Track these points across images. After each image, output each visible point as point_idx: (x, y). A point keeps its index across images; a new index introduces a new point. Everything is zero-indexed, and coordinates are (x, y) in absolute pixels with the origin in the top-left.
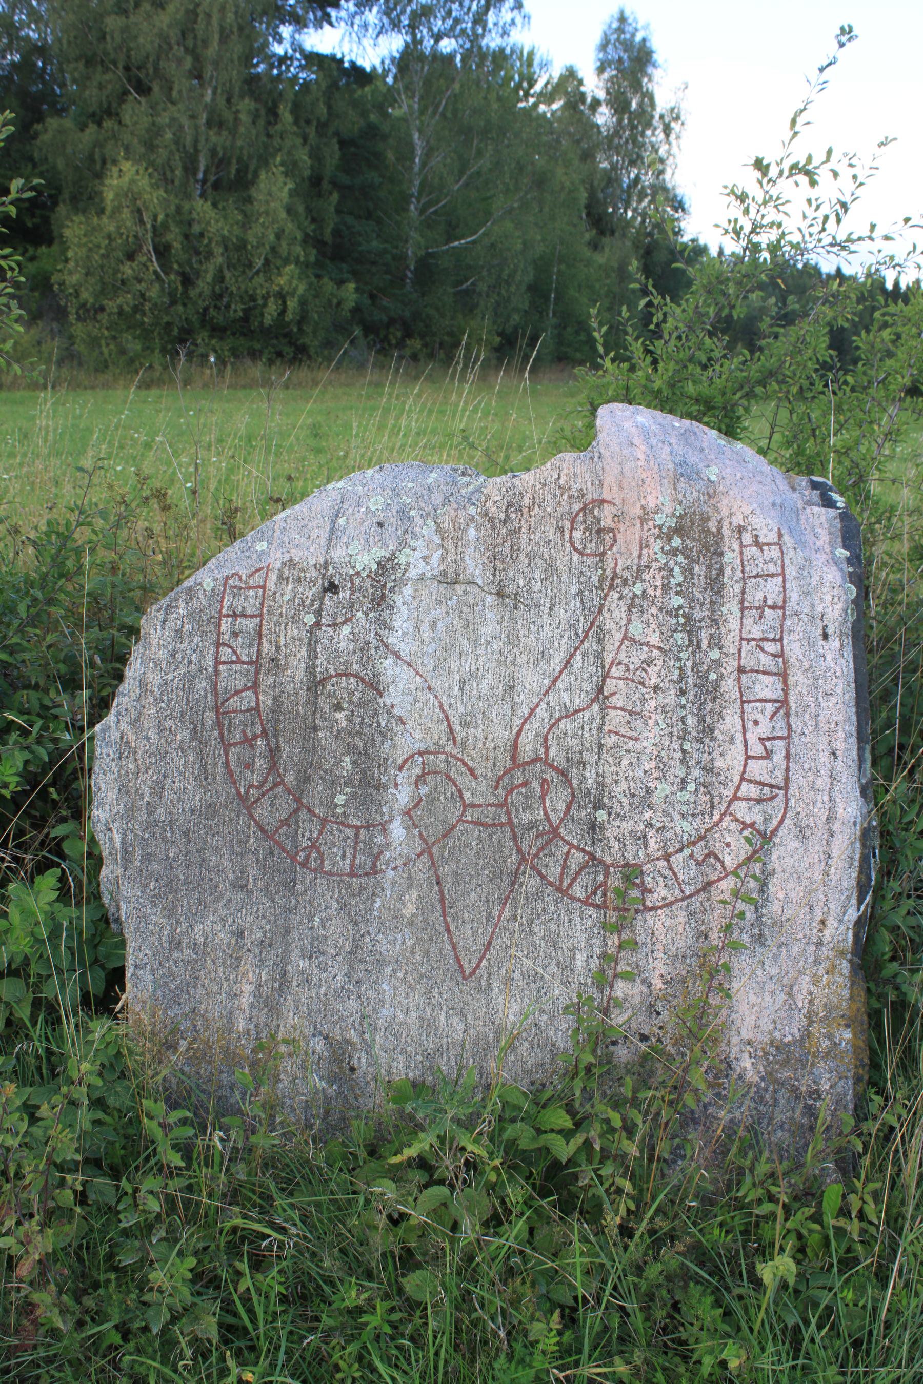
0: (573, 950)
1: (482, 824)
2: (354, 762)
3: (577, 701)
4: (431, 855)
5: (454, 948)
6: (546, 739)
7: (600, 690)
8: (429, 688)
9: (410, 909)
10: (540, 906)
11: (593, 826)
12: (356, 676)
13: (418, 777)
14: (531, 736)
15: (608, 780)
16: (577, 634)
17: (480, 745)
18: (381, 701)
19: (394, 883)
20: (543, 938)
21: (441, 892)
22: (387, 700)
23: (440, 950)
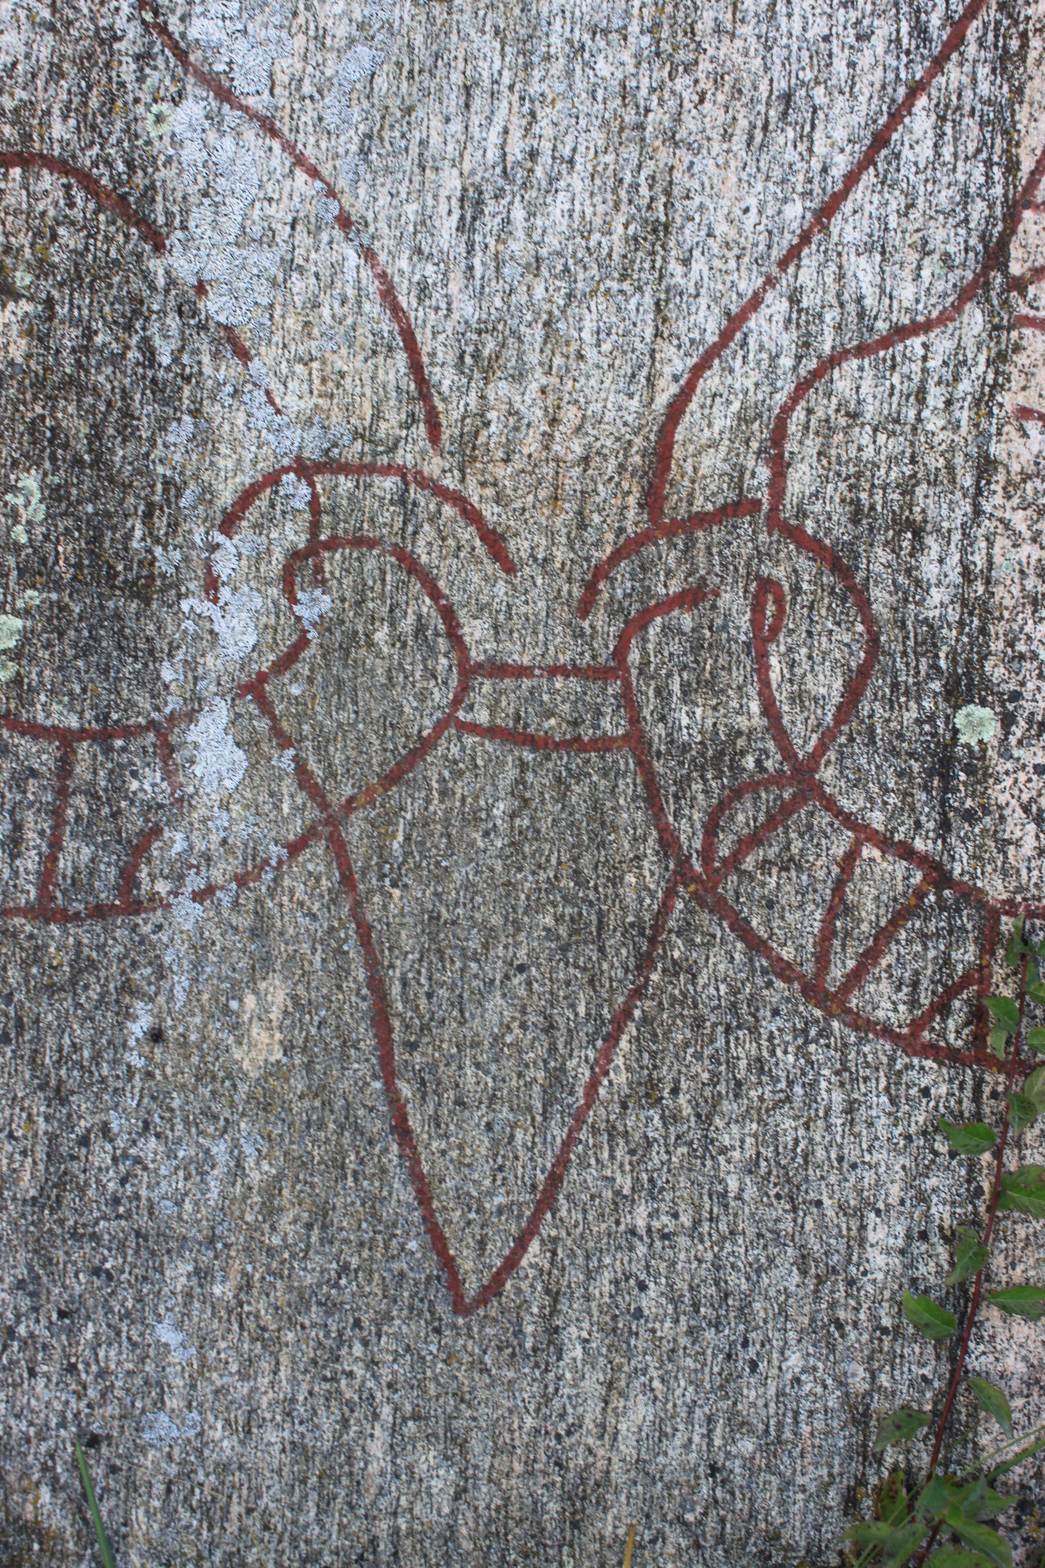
0: (860, 1210)
1: (532, 742)
2: (54, 495)
3: (907, 293)
4: (339, 849)
5: (424, 1197)
6: (779, 434)
7: (996, 254)
8: (344, 221)
9: (259, 1049)
10: (745, 1050)
11: (946, 764)
12: (62, 166)
13: (295, 556)
14: (722, 420)
15: (1006, 595)
16: (920, 31)
17: (531, 444)
18: (156, 266)
19: (200, 948)
20: (751, 1168)
21: (377, 986)
22: (182, 264)
23: (373, 1204)
